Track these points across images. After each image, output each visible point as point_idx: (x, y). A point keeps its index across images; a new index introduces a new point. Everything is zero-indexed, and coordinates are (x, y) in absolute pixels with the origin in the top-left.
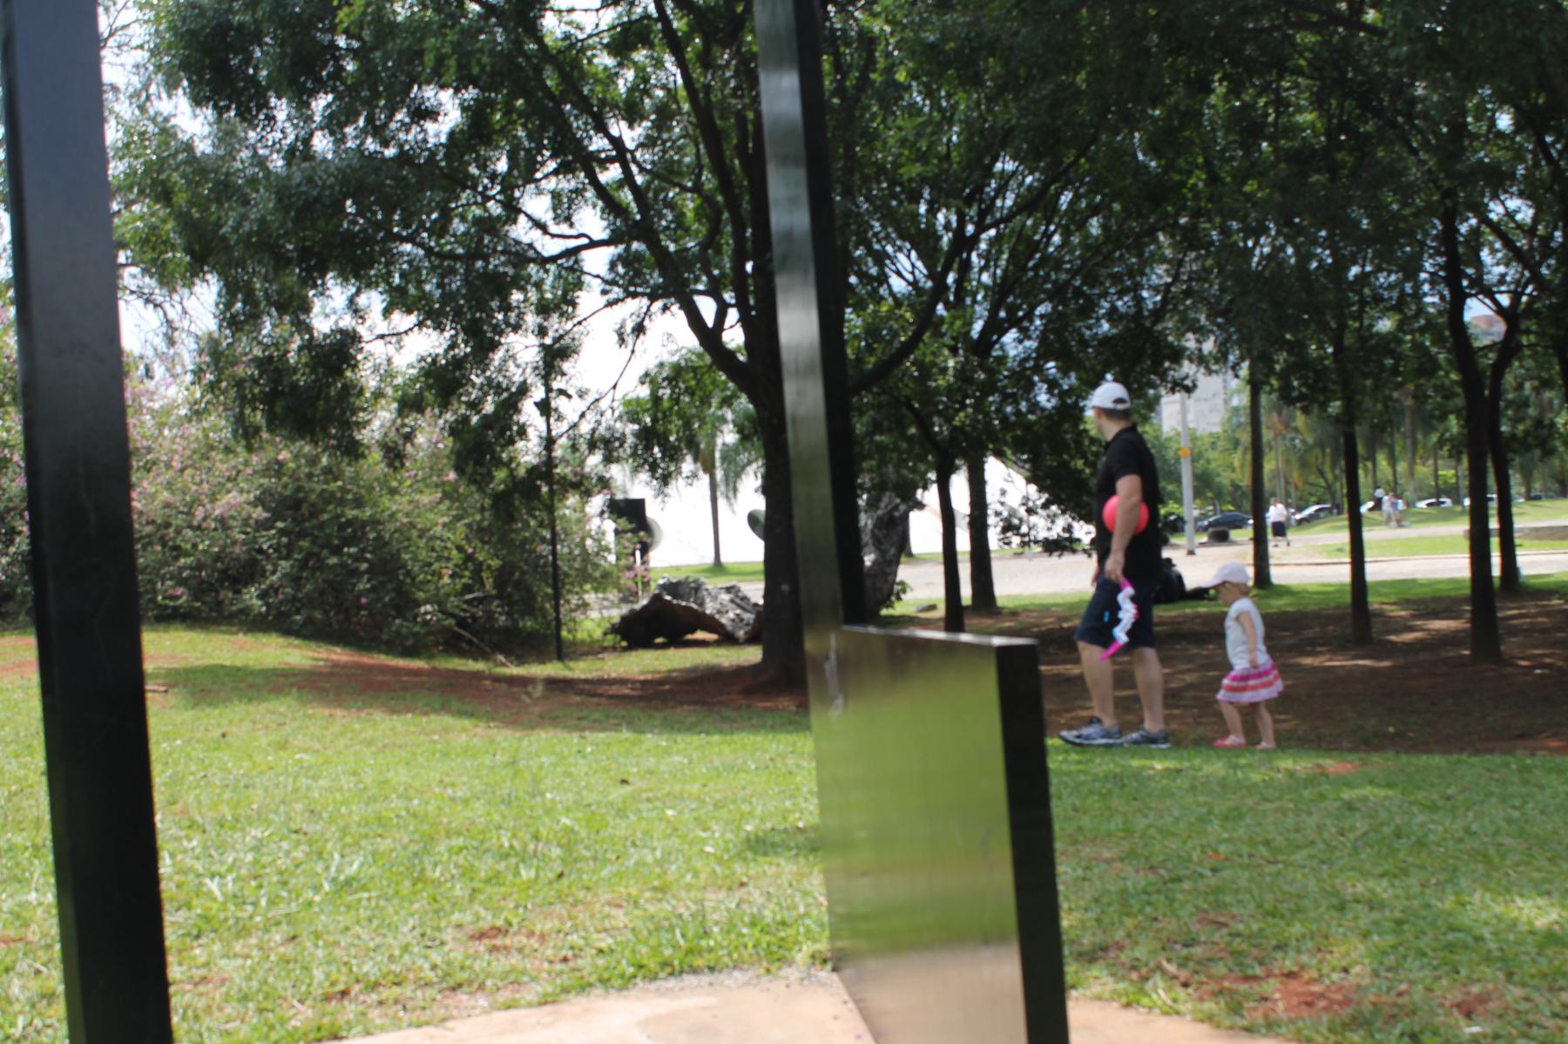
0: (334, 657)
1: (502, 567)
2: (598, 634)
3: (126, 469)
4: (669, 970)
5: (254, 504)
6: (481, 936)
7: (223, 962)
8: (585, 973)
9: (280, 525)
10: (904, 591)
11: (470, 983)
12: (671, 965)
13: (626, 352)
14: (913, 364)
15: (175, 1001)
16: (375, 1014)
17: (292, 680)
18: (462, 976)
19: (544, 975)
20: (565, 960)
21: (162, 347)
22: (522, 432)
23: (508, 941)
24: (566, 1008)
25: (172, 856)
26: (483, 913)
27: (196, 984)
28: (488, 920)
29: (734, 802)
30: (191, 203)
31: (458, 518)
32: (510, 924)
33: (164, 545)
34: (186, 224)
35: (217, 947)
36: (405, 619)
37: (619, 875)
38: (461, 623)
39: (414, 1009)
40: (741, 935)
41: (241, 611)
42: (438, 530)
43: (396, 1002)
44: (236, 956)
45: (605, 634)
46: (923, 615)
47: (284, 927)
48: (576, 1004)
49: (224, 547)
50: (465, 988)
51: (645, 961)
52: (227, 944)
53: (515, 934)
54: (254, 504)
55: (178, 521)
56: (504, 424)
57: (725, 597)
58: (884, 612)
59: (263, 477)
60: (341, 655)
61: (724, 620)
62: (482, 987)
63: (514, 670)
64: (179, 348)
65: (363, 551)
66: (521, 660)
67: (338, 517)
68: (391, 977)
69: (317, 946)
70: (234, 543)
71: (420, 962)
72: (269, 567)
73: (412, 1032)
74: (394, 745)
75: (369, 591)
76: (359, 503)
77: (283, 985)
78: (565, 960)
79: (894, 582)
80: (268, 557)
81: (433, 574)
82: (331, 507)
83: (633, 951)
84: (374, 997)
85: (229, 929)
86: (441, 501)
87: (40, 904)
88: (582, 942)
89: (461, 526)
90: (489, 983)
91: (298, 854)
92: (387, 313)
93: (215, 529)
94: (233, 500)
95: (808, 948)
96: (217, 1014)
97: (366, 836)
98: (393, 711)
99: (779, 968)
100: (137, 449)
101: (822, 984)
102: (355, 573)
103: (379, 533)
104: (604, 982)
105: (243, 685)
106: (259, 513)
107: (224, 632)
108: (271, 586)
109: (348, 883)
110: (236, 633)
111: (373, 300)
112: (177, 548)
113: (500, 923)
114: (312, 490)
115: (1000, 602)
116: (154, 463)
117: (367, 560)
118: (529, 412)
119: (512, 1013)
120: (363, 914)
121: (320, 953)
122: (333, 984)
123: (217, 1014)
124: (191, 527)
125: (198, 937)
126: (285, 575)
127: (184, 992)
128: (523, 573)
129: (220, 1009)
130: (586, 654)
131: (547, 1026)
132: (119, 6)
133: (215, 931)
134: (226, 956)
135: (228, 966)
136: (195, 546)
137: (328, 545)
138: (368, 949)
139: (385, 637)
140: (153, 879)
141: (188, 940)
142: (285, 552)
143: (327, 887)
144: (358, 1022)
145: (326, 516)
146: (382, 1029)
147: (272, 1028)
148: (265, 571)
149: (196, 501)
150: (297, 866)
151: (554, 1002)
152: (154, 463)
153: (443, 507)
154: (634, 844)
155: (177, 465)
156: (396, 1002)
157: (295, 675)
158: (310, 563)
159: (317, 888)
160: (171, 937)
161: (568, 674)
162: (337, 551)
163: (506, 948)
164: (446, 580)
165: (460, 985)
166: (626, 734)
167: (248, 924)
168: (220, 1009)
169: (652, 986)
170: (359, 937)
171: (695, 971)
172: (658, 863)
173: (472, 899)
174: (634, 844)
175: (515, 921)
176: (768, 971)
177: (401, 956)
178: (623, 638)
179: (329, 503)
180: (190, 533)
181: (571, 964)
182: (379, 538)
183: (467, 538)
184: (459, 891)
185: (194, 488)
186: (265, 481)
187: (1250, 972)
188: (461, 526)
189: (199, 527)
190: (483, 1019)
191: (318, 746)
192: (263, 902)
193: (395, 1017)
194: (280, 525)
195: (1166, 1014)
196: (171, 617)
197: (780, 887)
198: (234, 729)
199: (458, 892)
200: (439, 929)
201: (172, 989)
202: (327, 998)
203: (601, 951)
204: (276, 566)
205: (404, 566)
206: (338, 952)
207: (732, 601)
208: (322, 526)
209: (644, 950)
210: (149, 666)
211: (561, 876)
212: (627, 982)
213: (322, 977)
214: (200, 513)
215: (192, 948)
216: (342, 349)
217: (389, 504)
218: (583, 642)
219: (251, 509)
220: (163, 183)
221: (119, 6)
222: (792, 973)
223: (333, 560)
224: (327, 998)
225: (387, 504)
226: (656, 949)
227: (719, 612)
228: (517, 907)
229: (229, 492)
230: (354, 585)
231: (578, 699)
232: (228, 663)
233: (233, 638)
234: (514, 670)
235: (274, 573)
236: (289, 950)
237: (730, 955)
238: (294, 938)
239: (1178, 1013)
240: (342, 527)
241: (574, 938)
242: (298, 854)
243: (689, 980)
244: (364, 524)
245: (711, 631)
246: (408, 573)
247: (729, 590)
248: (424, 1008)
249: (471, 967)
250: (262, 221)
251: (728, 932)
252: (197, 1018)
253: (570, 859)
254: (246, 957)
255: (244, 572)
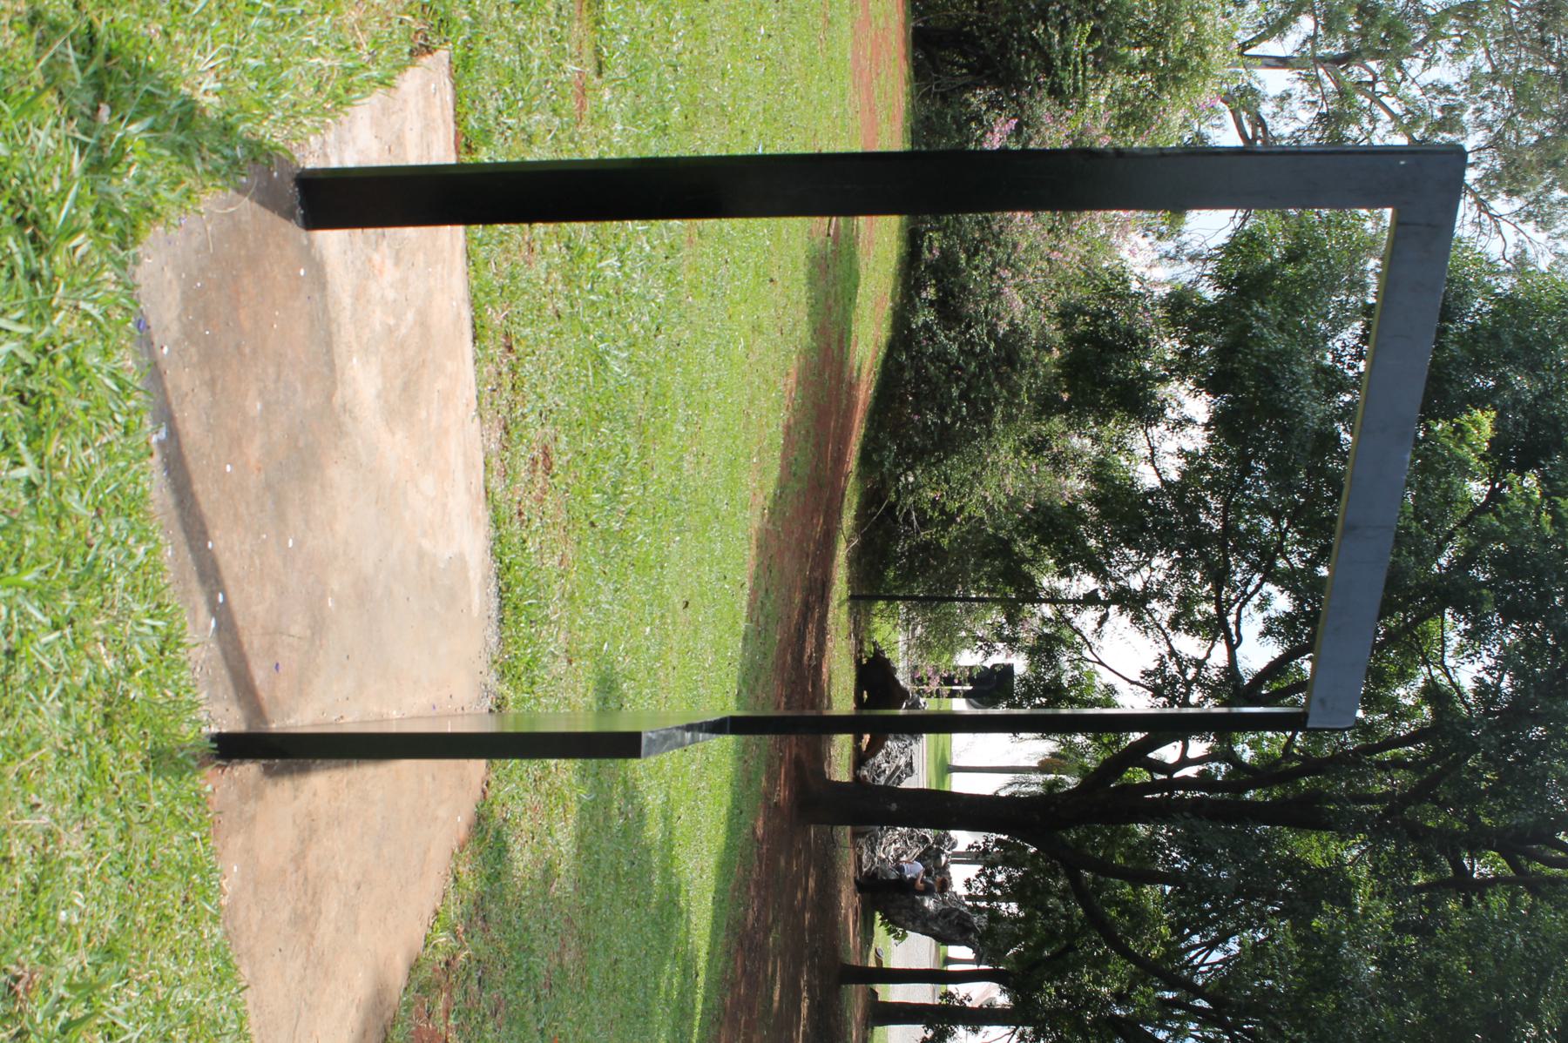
0: (863, 387)
1: (942, 549)
2: (877, 637)
3: (1052, 207)
4: (504, 588)
5: (1011, 323)
6: (546, 455)
7: (544, 263)
8: (507, 526)
9: (992, 346)
10: (895, 938)
11: (509, 440)
12: (508, 591)
13: (1136, 677)
14: (1105, 952)
15: (515, 228)
16: (492, 368)
17: (835, 346)
18: (515, 436)
19: (510, 496)
20: (520, 514)
21: (1189, 250)
22: (1066, 573)
23: (539, 473)
24: (481, 506)
25: (646, 232)
26: (565, 458)
27: (529, 244)
28: (558, 462)
29: (653, 685)
30: (1285, 280)
31: (990, 511)
32: (552, 477)
33: (982, 241)
34: (1270, 273)
35: (557, 260)
36: (896, 455)
37: (589, 569)
38: (892, 507)
39: (491, 397)
40: (526, 647)
41: (914, 306)
42: (979, 490)
43: (499, 385)
44: (549, 274)
45: (875, 644)
46: (872, 953)
47: (569, 310)
48: (484, 515)
49: (974, 295)
50: (504, 436)
51: (512, 571)
52: (559, 268)
53: (545, 480)
54: (1011, 323)
55: (1001, 254)
56: (1073, 557)
57: (902, 761)
58: (878, 916)
59: (1038, 334)
60: (865, 393)
61: (880, 757)
62: (505, 448)
63: (842, 552)
64: (1188, 265)
65: (963, 420)
66: (853, 560)
67: (996, 399)
68: (519, 383)
69: (550, 333)
70: (977, 303)
71: (529, 406)
72: (953, 334)
73: (474, 393)
74: (749, 423)
75: (925, 424)
76: (1009, 419)
77: (521, 304)
78: (520, 514)
79: (905, 928)
80: (963, 333)
81: (938, 484)
82: (1005, 393)
83: (521, 565)
84: (505, 370)
85: (572, 270)
86: (1007, 495)
87: (611, 132)
88: (533, 528)
89: (982, 513)
90: (507, 454)
91: (635, 328)
92: (1182, 453)
93: (991, 287)
94: (1015, 305)
95: (511, 695)
96: (503, 257)
97: (648, 382)
98: (788, 429)
99: (496, 670)
100: (1071, 221)
101: (480, 699)
102: (942, 411)
103: (979, 435)
104: (499, 539)
105: (831, 302)
106: (1003, 328)
107: (894, 289)
108: (935, 334)
109: (603, 362)
110: (893, 299)
111: (1196, 440)
112: (976, 253)
113: (555, 469)
114: (1021, 377)
115: (878, 1030)
116: (1057, 236)
117: (954, 423)
118: (1087, 583)
119: (481, 467)
120: (574, 370)
121: (544, 334)
122: (517, 341)
123: (503, 257)
124: (994, 265)
125: (568, 247)
126: (945, 347)
127: (522, 235)
128: (936, 569)
129: (506, 259)
130: (856, 623)
131: (468, 490)
132: (1519, 225)
133: (571, 260)
134: (549, 266)
135: (540, 267)
136: (977, 268)
137: (970, 387)
138: (543, 370)
139: (881, 435)
140: (632, 217)
141: (566, 240)
142: (968, 349)
143: (601, 346)
144: (486, 355)
145: (997, 388)
146: (478, 372)
147: (487, 294)
148: (950, 330)
149: (1018, 271)
150: (625, 327)
151: (487, 498)
152: (1057, 236)
153: (1002, 497)
154: (617, 590)
155: (1054, 256)
156: (499, 385)
157: (841, 349)
158: (953, 371)
159: (602, 339)
160: (567, 227)
161: (834, 603)
162: (964, 396)
163: (534, 471)
164: (931, 495)
165: (508, 433)
166: (742, 625)
167: (573, 284)
168: (506, 259)
169: (492, 573)
170: (553, 364)
171: (501, 608)
172: (597, 604)
173: (578, 453)
174: (617, 590)
175: (555, 480)
176: (495, 662)
177: (535, 393)
178: (869, 660)
179: (1009, 392)
180: (989, 264)
181: (516, 517)
182: (975, 436)
183: (970, 518)
184: (587, 444)
185: (1030, 270)
186: (1034, 335)
187: (452, 1016)
188: (982, 513)
189: (993, 272)
190: (479, 446)
191: (752, 359)
192: (593, 297)
193: (487, 383)
194: (992, 346)
195: (426, 937)
196: (913, 242)
197: (566, 690)
198: (779, 290)
199: (586, 443)
200: (555, 423)
201: (526, 226)
202: (507, 336)
203: (524, 542)
204: (955, 339)
205: (946, 457)
206: (543, 348)
207: (898, 767)
208: (989, 385)
209: (522, 574)
210: (862, 220)
211: (592, 524)
212: (498, 556)
213: (524, 334)
214: (1007, 274)
215: (558, 242)
216: (1145, 410)
217: (1006, 448)
218: (869, 622)
219: (1007, 319)
220: (1305, 254)
221: (1519, 225)
222: (492, 679)
223: (955, 392)
224: (507, 336)
225: (1006, 446)
226: (521, 582)
227: (888, 754)
228: (567, 484)
229: (1025, 301)
230: (931, 410)
231: (797, 599)
232: (860, 290)
233: (888, 296)
234: (842, 552)
235: (946, 336)
236: (549, 312)
237: (511, 636)
238: (559, 316)
239: (426, 946)
240: (986, 402)
241: (537, 523)
242: (635, 328)
243: (495, 603)
244: (987, 422)
245: (868, 746)
246: (940, 461)
247: (910, 765)
248: (492, 404)
249: (521, 442)
250: (1262, 338)
251: (529, 639)
252: (501, 242)
253: (606, 536)
254: (547, 282)
255: (949, 310)
